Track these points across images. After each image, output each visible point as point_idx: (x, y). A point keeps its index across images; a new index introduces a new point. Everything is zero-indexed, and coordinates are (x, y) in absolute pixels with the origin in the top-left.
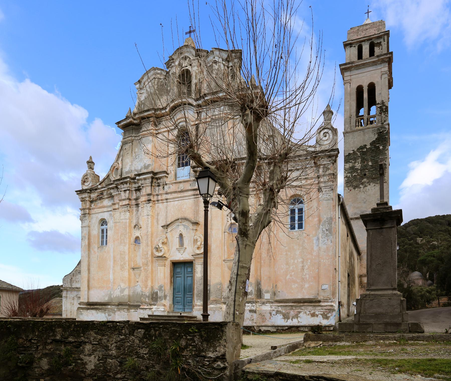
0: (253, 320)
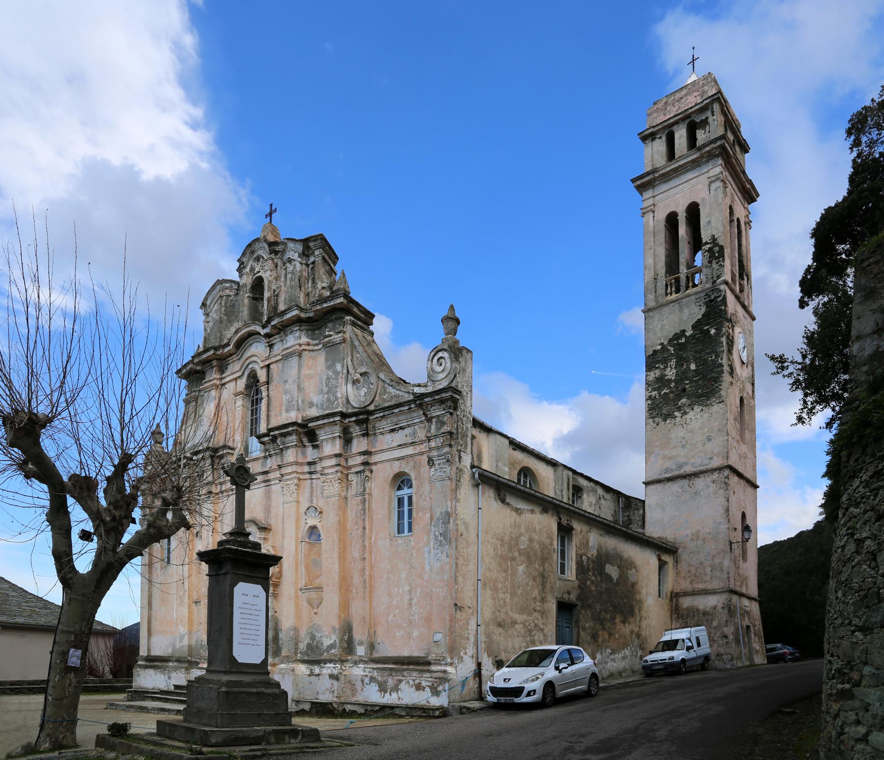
0: (333, 691)
